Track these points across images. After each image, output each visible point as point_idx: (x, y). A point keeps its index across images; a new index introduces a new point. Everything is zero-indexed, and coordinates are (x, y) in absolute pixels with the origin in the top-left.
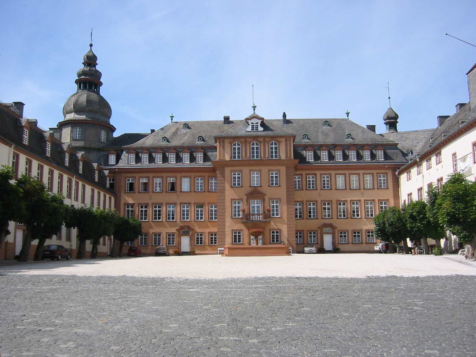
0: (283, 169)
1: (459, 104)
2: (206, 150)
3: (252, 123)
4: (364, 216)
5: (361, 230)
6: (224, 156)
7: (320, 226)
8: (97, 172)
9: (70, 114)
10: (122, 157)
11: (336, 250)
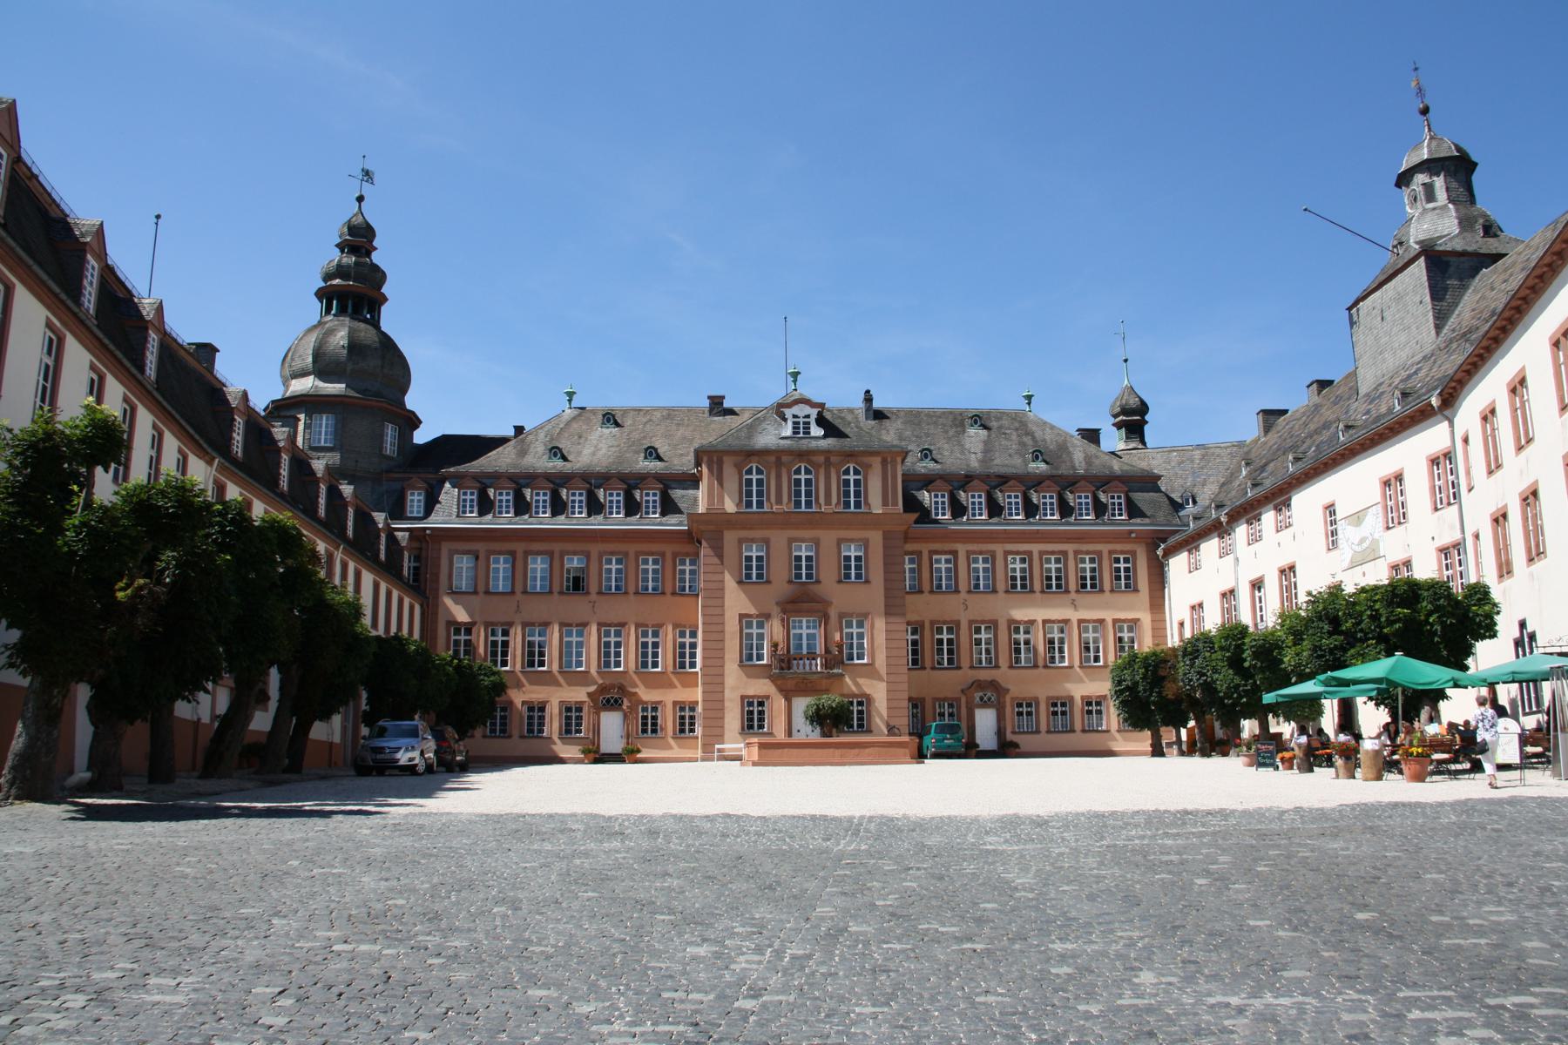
0: (876, 538)
1: (1317, 381)
2: (669, 486)
3: (795, 416)
4: (1077, 663)
5: (1071, 699)
6: (722, 501)
7: (964, 687)
8: (383, 535)
9: (303, 380)
10: (442, 497)
11: (1006, 749)
